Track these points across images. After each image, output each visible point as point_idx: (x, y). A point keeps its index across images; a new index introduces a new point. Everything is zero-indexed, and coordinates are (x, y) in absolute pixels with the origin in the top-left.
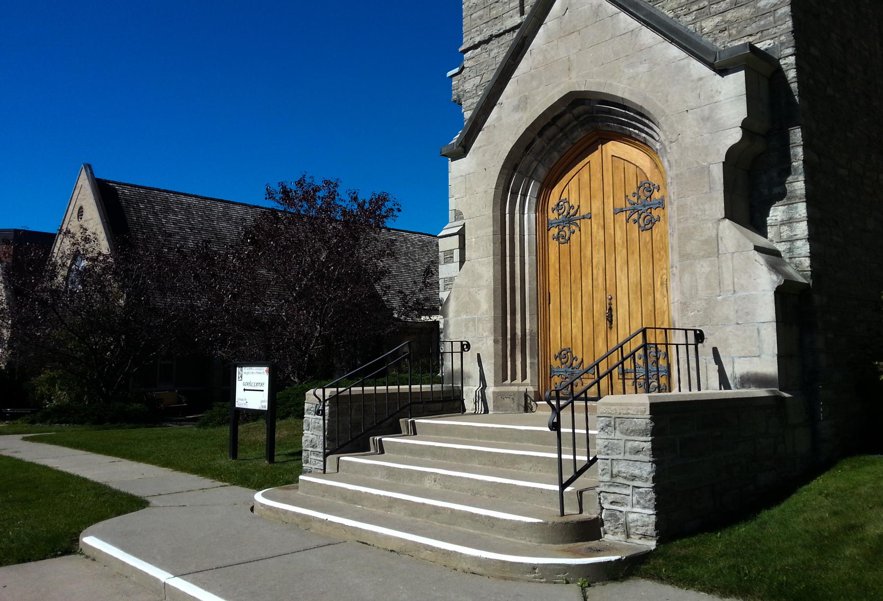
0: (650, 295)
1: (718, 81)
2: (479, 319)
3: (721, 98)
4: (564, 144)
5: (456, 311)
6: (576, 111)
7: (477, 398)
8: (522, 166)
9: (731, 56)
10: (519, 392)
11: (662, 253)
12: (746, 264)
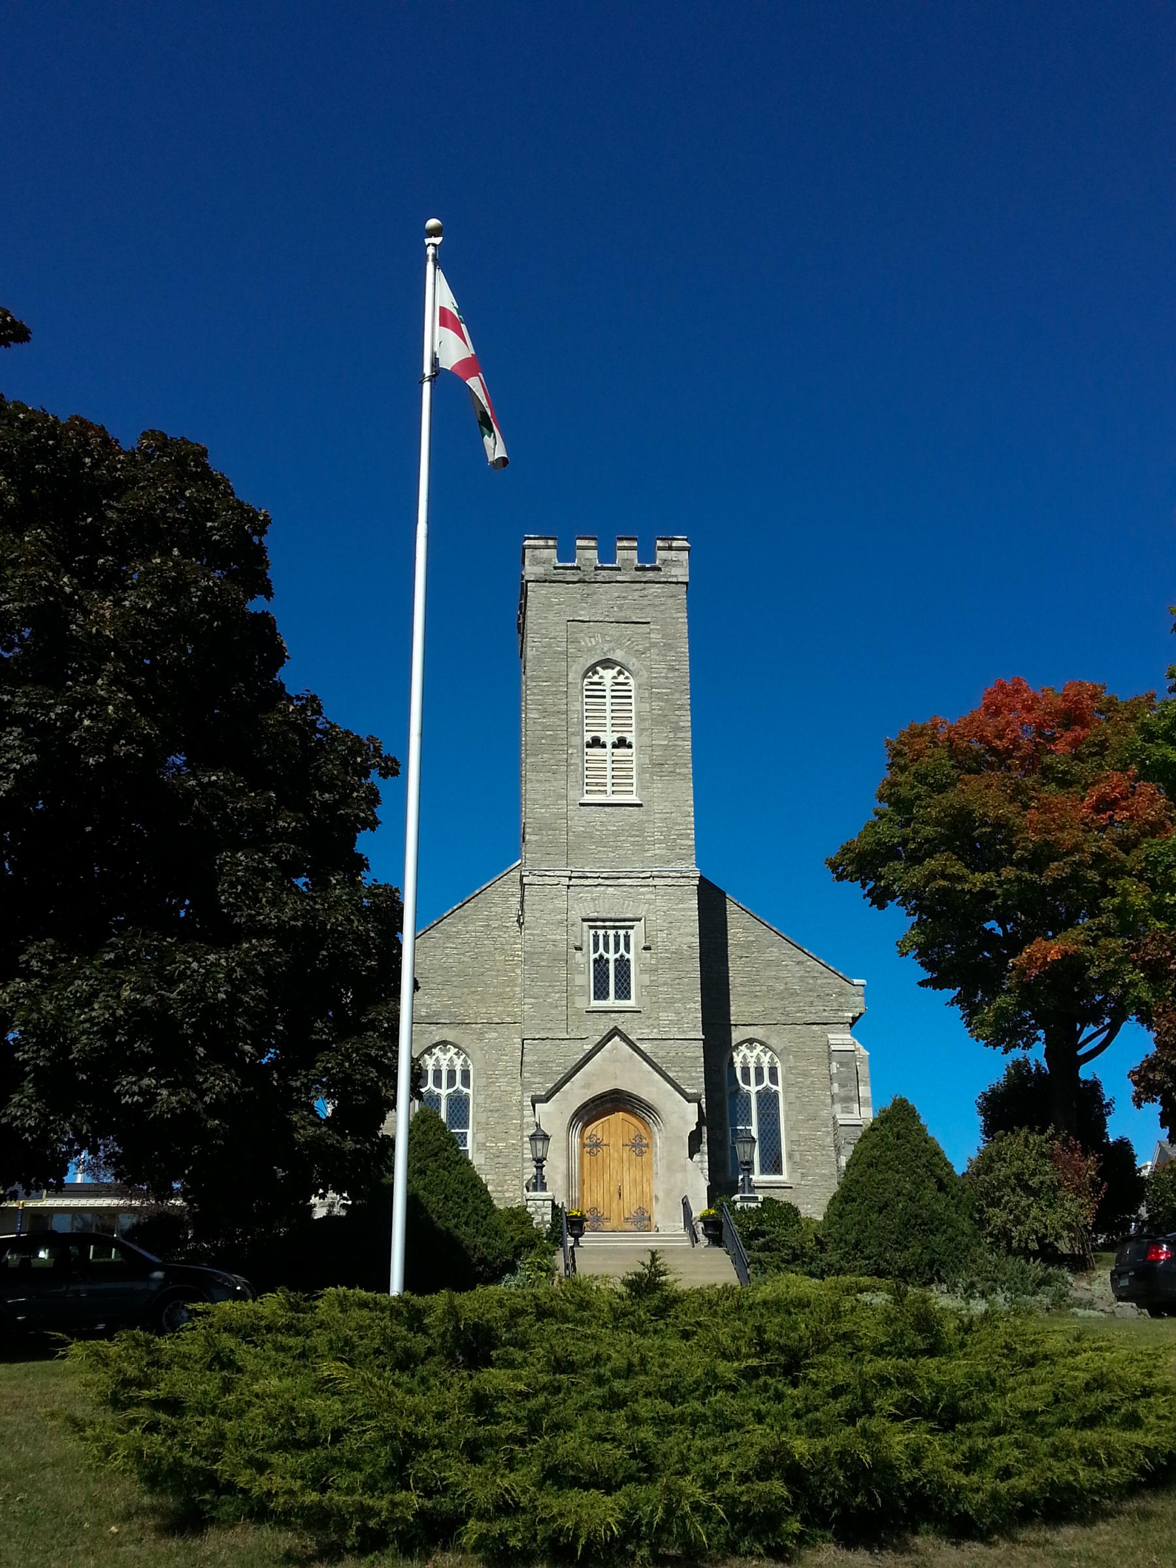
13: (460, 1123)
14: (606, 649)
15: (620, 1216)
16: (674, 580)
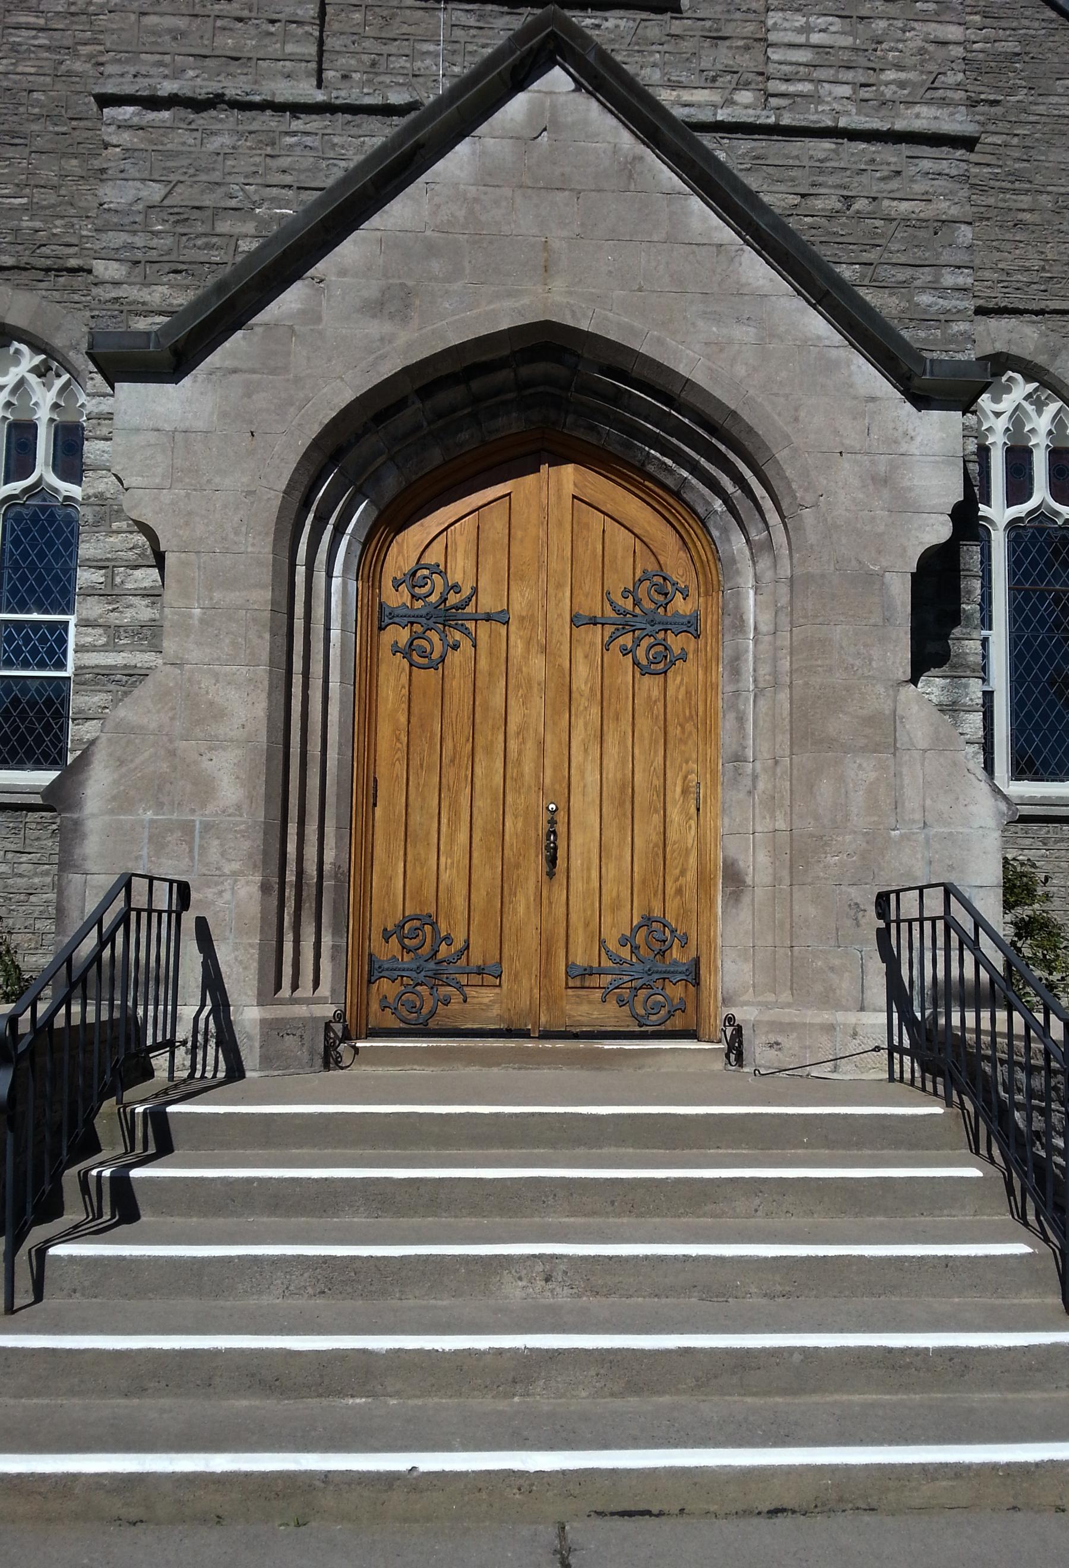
0: (656, 811)
1: (909, 415)
2: (207, 827)
3: (914, 448)
4: (464, 436)
5: (114, 798)
6: (525, 371)
7: (200, 1038)
9: (954, 376)
10: (315, 1019)
11: (689, 727)
12: (949, 775)
13: (48, 592)
15: (547, 955)
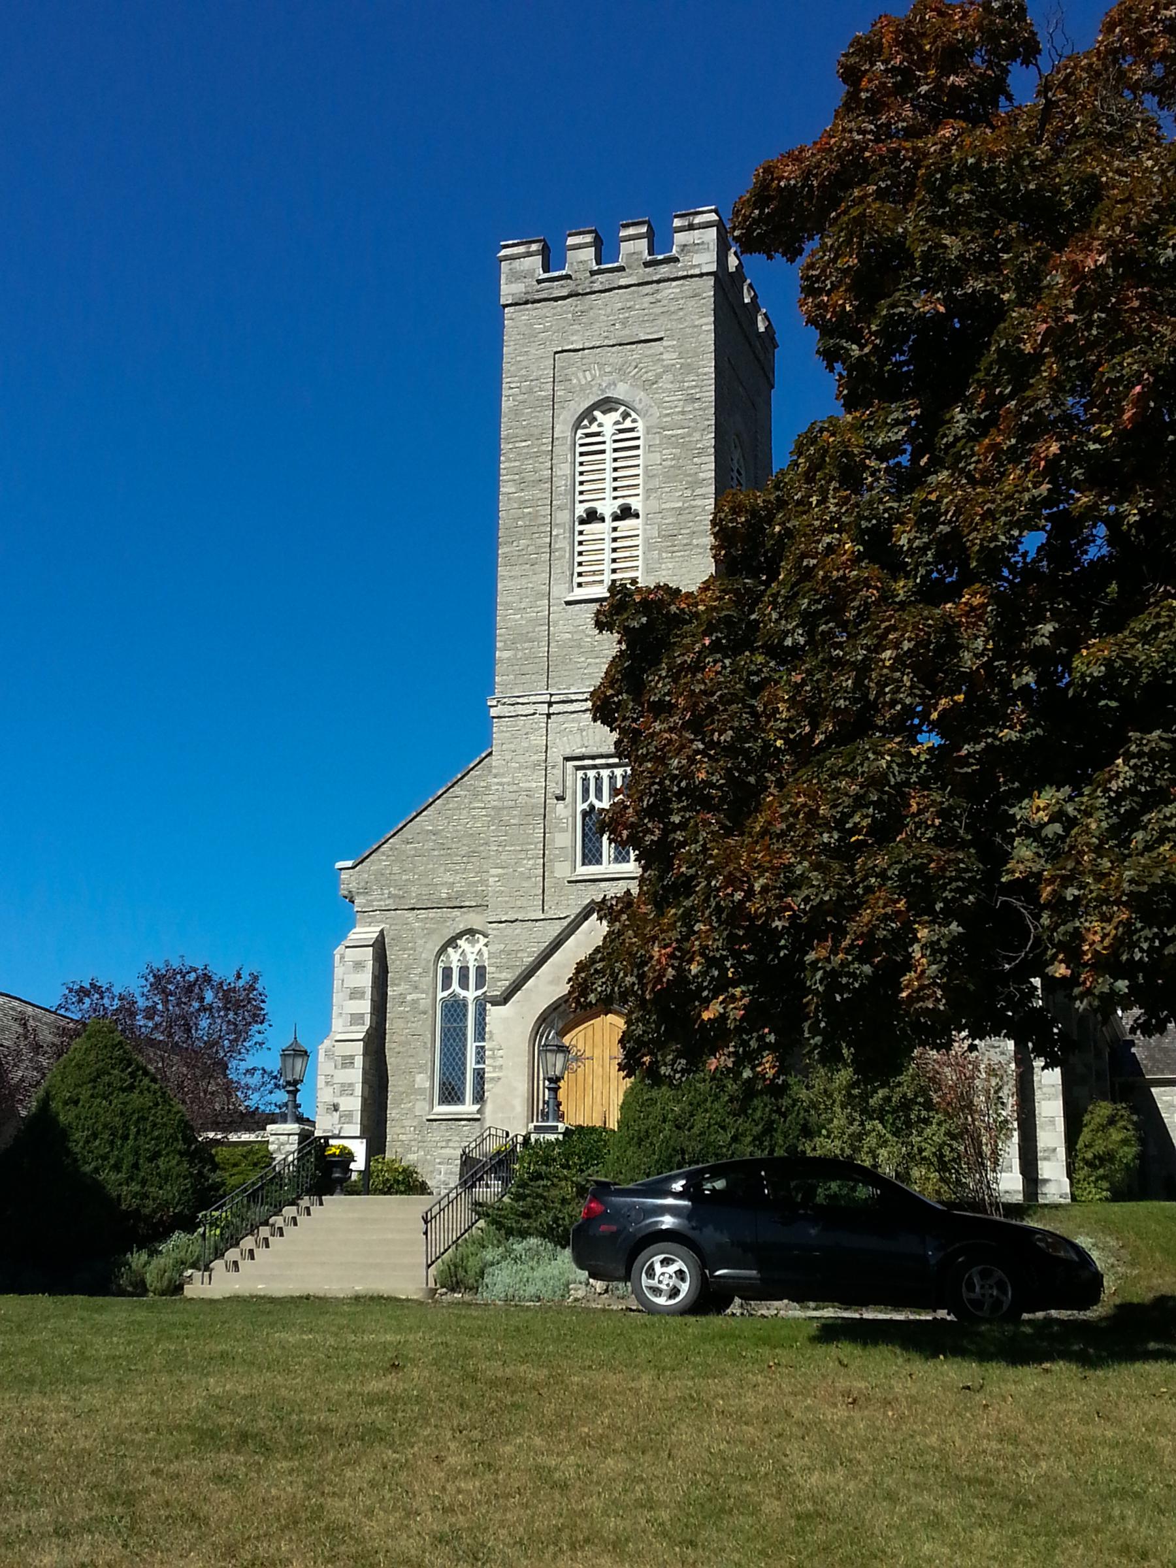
8: (548, 1020)
14: (604, 385)
16: (697, 271)
